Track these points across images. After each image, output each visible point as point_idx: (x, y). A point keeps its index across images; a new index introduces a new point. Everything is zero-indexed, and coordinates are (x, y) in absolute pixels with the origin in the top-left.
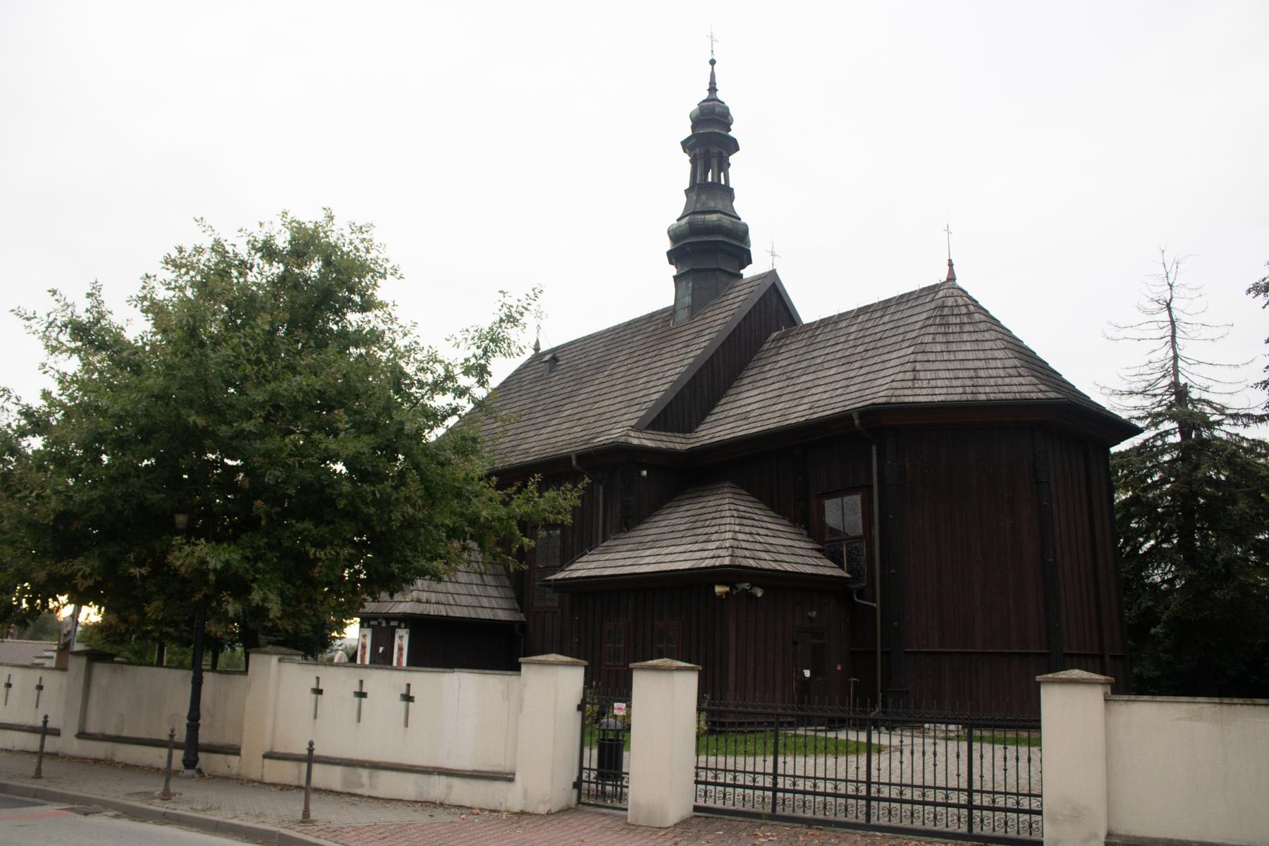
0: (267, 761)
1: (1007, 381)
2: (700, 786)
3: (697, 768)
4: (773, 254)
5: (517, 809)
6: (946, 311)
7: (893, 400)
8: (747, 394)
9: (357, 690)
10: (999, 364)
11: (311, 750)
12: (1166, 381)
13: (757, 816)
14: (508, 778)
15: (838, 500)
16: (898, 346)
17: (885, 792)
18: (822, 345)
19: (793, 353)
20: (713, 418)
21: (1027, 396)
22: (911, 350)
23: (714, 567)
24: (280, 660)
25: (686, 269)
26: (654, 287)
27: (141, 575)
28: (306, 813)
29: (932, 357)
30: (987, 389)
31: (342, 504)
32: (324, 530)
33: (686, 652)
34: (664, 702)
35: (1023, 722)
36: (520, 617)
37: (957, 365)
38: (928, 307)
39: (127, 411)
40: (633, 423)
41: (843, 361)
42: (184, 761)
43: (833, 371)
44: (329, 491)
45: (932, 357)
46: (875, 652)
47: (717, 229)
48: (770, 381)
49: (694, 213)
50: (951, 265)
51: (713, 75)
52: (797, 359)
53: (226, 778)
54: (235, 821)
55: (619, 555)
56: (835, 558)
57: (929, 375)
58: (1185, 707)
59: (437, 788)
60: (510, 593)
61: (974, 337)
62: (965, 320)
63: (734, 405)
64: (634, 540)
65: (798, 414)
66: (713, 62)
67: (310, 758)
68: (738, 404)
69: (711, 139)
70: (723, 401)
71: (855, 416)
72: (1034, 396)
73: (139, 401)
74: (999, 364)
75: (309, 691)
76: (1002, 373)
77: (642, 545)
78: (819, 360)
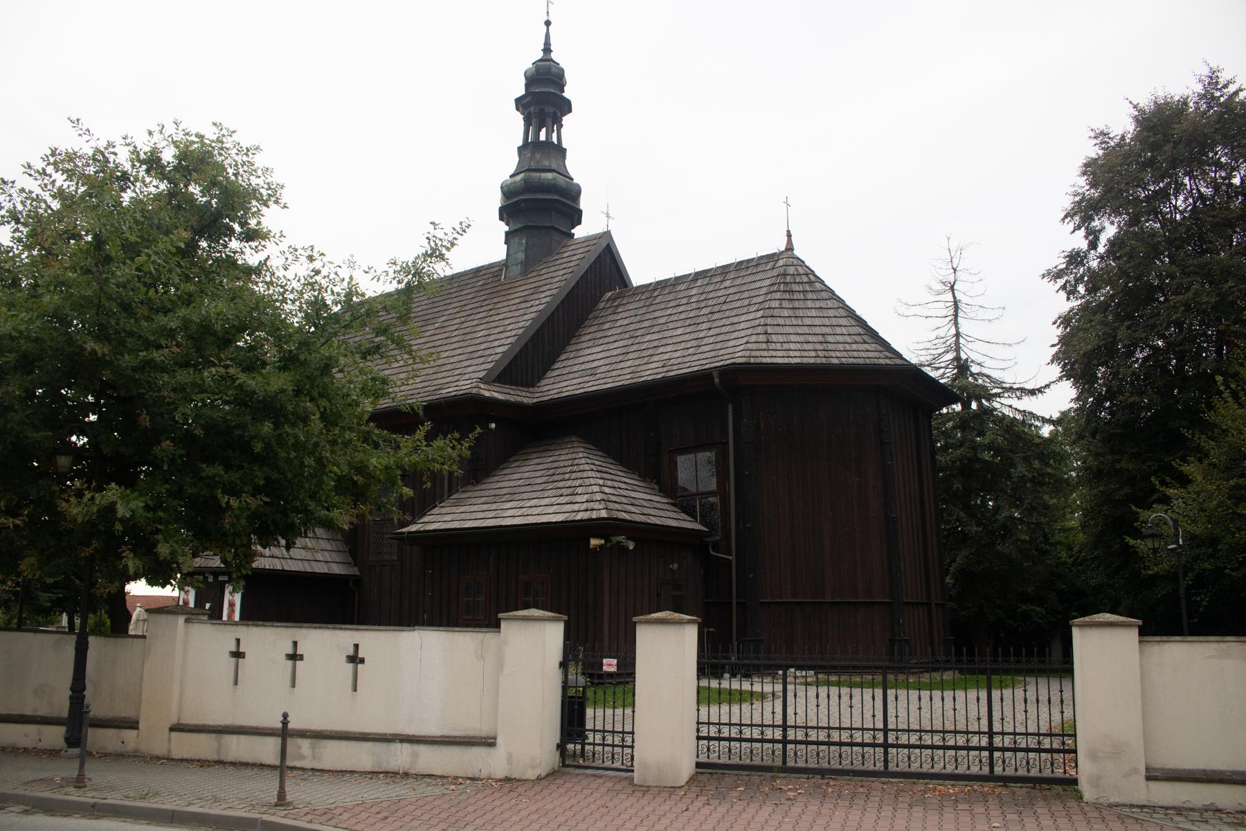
0: (173, 734)
1: (854, 347)
2: (701, 742)
3: (698, 723)
4: (608, 216)
5: (500, 774)
6: (788, 279)
7: (752, 360)
8: (589, 351)
9: (290, 652)
10: (844, 331)
11: (285, 722)
12: (951, 356)
13: (768, 769)
14: (489, 742)
15: (691, 456)
16: (745, 310)
17: (904, 739)
18: (663, 306)
19: (632, 313)
20: (555, 373)
21: (876, 361)
22: (760, 313)
23: (591, 520)
24: (187, 621)
25: (519, 226)
26: (486, 244)
27: (16, 526)
28: (282, 795)
29: (781, 321)
30: (838, 354)
31: (258, 447)
32: (235, 476)
33: (553, 604)
34: (667, 652)
35: (1064, 668)
36: (354, 571)
37: (805, 330)
38: (769, 274)
39: (20, 332)
40: (482, 374)
41: (688, 322)
42: (66, 739)
43: (680, 331)
44: (238, 432)
45: (781, 321)
46: (730, 603)
47: (551, 188)
48: (612, 339)
49: (529, 170)
50: (789, 235)
51: (547, 36)
52: (638, 318)
53: (120, 756)
54: (192, 809)
55: (474, 508)
56: (688, 510)
57: (781, 338)
58: (1215, 645)
59: (400, 756)
60: (341, 546)
61: (818, 304)
62: (808, 288)
63: (577, 361)
64: (488, 493)
65: (651, 371)
66: (548, 23)
67: (285, 733)
68: (581, 360)
69: (544, 97)
70: (563, 357)
71: (715, 374)
72: (882, 361)
73: (31, 321)
74: (844, 331)
75: (227, 654)
76: (848, 339)
77: (497, 498)
78: (663, 320)
